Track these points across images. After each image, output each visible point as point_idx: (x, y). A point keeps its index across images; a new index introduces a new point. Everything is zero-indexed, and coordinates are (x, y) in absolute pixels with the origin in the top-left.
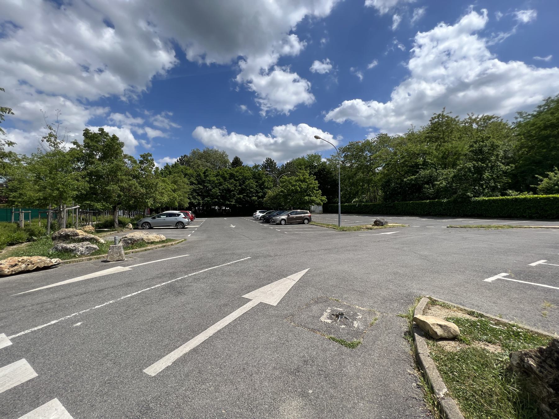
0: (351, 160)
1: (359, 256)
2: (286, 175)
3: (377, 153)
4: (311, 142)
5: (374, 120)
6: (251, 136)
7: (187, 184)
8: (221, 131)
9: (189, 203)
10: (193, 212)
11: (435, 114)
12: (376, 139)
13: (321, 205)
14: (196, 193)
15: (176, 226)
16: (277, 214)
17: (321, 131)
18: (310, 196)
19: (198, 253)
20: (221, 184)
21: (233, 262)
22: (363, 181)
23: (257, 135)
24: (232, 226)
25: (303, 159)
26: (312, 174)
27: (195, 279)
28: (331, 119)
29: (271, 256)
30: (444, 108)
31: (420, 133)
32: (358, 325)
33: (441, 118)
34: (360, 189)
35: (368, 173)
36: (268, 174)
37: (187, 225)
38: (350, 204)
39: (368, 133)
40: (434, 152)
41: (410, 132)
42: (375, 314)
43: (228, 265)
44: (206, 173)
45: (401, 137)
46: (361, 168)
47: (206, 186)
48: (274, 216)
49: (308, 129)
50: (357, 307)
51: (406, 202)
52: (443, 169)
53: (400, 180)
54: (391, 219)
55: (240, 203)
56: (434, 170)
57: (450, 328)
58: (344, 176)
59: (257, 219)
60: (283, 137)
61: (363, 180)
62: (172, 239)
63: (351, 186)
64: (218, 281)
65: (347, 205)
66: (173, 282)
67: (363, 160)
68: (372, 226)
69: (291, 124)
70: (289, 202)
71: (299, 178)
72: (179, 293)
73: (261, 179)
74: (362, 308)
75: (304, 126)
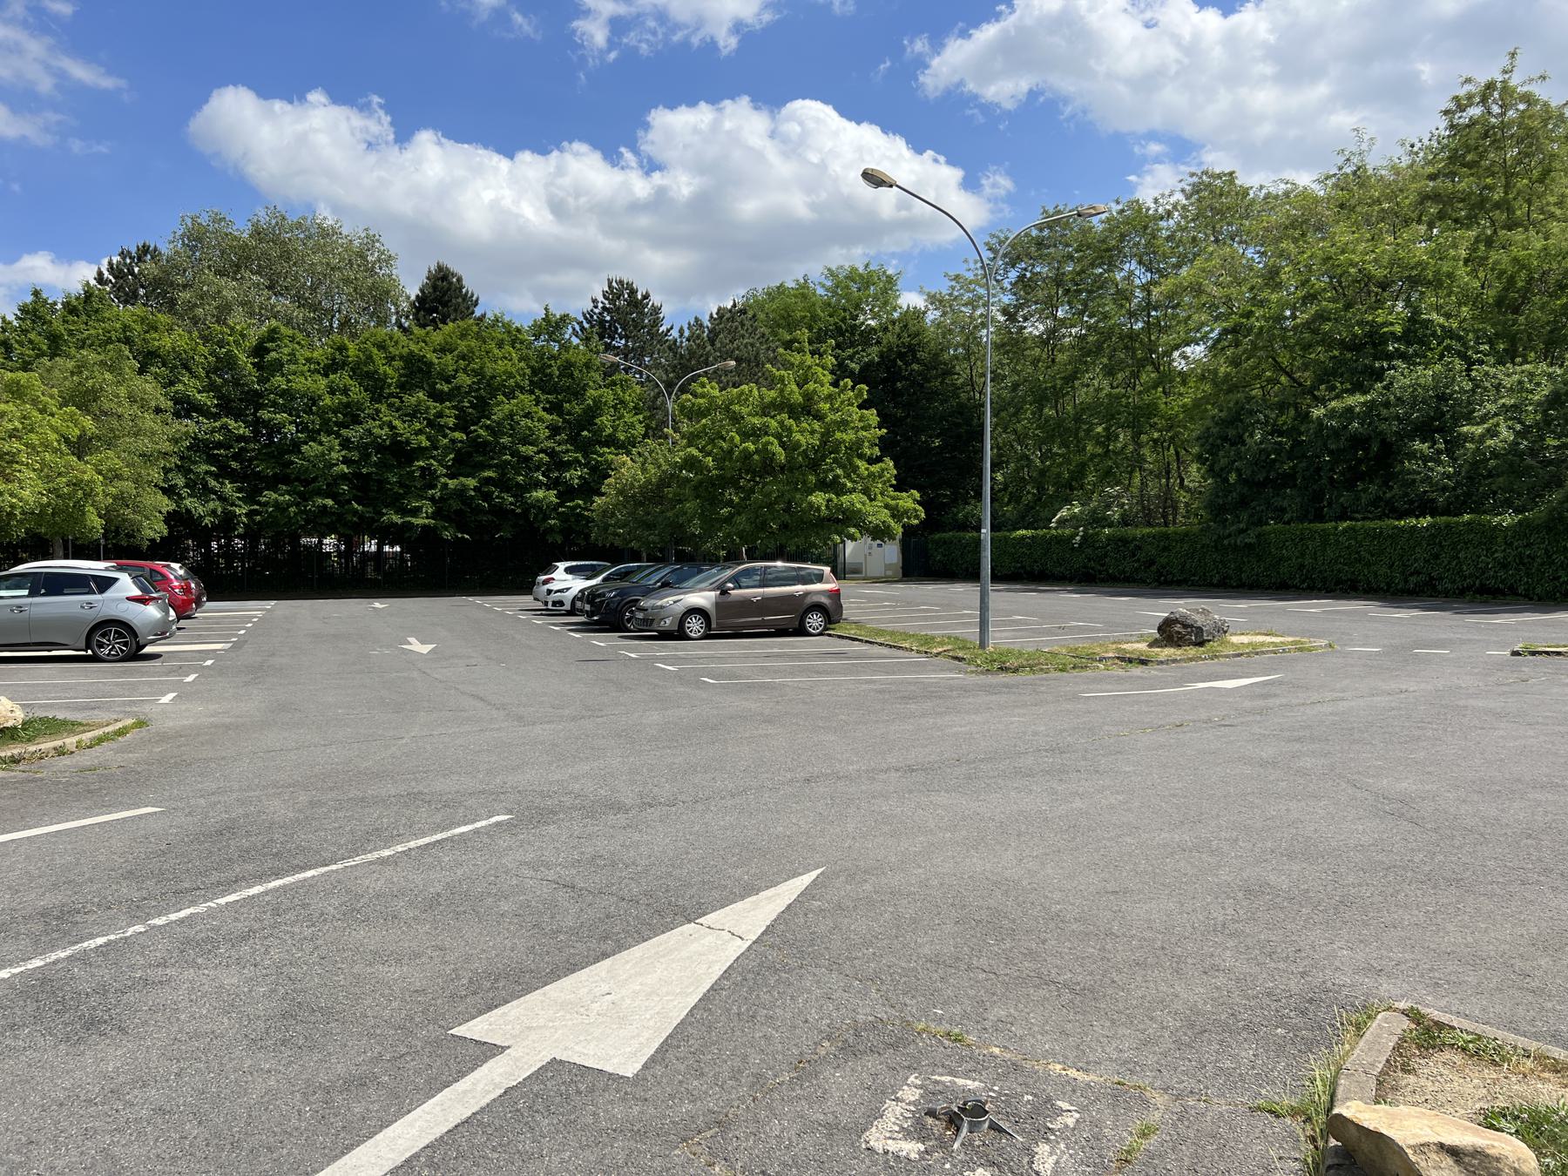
0: (1050, 304)
1: (1078, 804)
2: (715, 376)
3: (1184, 271)
4: (848, 203)
5: (1171, 96)
6: (526, 156)
7: (158, 410)
8: (357, 120)
9: (170, 518)
10: (194, 570)
11: (1468, 81)
12: (1179, 197)
13: (892, 537)
14: (212, 459)
15: (88, 646)
16: (666, 585)
17: (899, 145)
18: (835, 487)
19: (213, 798)
20: (352, 415)
21: (412, 844)
22: (1110, 417)
23: (561, 150)
24: (417, 646)
25: (803, 291)
26: (851, 375)
27: (188, 941)
28: (956, 79)
29: (618, 808)
30: (1513, 55)
31: (1398, 174)
32: (1057, 1162)
33: (1495, 102)
34: (1093, 456)
35: (1136, 375)
36: (616, 367)
37: (152, 642)
38: (1041, 532)
39: (1140, 165)
40: (1462, 271)
41: (1348, 170)
42: (1145, 1103)
43: (383, 861)
44: (268, 351)
45: (1305, 194)
46: (1098, 349)
47: (266, 424)
48: (648, 592)
49: (836, 134)
50: (1058, 1067)
51: (1320, 526)
52: (1501, 362)
53: (1292, 412)
54: (1242, 613)
55: (458, 520)
56: (1459, 364)
57: (1498, 1160)
58: (1015, 387)
59: (555, 609)
60: (700, 168)
61: (1109, 411)
62: (64, 723)
63: (1050, 439)
64: (323, 951)
65: (1023, 538)
66: (54, 963)
67: (1109, 307)
68: (1150, 646)
69: (745, 100)
70: (728, 520)
71: (782, 391)
72: (91, 1024)
73: (578, 393)
74: (1080, 1076)
75: (813, 113)
